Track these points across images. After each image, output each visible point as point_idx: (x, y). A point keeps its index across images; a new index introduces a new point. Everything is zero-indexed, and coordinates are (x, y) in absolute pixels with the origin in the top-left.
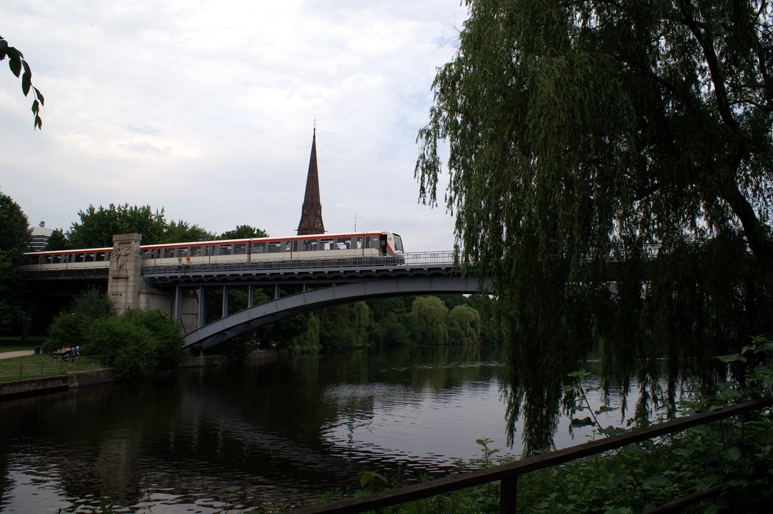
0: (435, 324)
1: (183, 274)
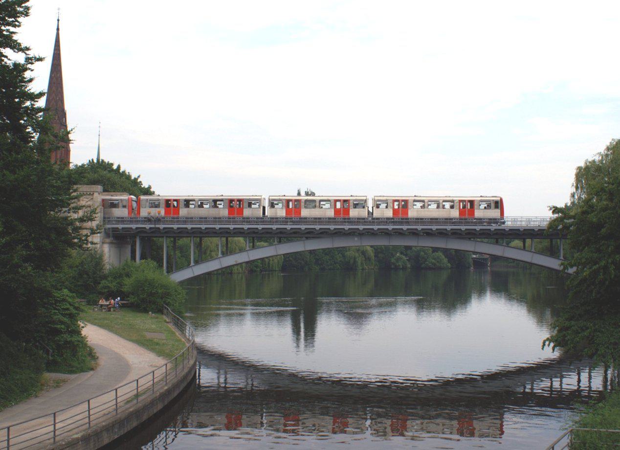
0: (208, 252)
1: (153, 226)
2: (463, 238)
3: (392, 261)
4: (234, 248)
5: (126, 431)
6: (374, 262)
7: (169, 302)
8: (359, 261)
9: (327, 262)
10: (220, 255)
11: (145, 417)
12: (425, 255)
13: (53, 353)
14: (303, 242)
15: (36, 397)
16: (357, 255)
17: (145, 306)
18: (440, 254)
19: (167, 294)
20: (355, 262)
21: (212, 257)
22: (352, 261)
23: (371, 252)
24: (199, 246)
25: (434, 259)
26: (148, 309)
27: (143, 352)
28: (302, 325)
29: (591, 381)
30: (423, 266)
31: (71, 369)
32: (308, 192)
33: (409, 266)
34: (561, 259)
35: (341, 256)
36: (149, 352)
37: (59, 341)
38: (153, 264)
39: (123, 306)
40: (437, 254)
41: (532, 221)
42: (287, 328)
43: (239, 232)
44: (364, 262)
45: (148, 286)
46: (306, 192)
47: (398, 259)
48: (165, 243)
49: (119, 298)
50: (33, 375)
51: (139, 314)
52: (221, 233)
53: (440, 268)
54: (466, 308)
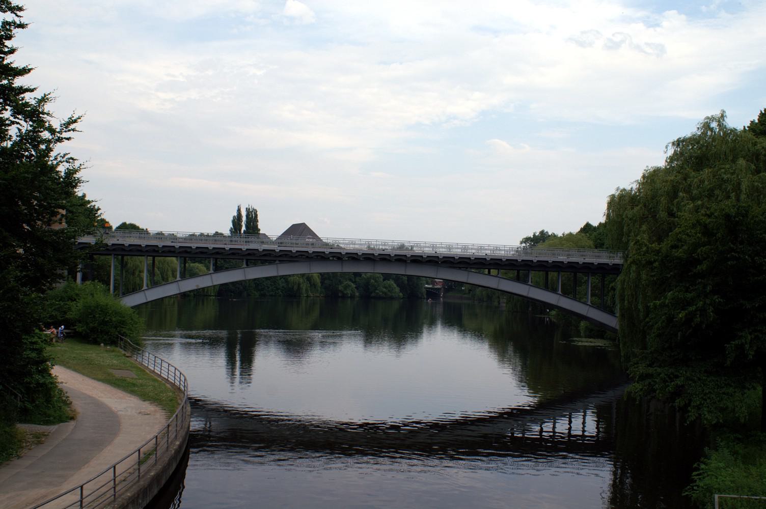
2: (454, 268)
3: (340, 289)
4: (166, 268)
5: (148, 502)
6: (319, 289)
7: (124, 333)
8: (304, 287)
9: (268, 288)
10: (178, 278)
11: (163, 482)
12: (376, 283)
13: (23, 398)
14: (275, 266)
15: (19, 457)
16: (301, 280)
17: (95, 336)
18: (392, 282)
19: (123, 323)
20: (299, 288)
21: (489, 272)
22: (296, 287)
23: (317, 278)
24: (123, 265)
25: (386, 288)
26: (99, 340)
27: (122, 395)
28: (238, 358)
29: (569, 426)
30: (373, 295)
31: (47, 419)
32: (249, 209)
33: (357, 294)
34: (559, 294)
35: (284, 281)
36: (129, 395)
37: (30, 383)
38: (100, 286)
39: (67, 337)
40: (389, 282)
41: (453, 248)
42: (220, 359)
44: (309, 288)
45: (100, 312)
46: (247, 208)
47: (347, 287)
48: (113, 263)
49: (63, 327)
50: (7, 428)
51: (89, 347)
52: (147, 251)
53: (392, 298)
54: (417, 341)
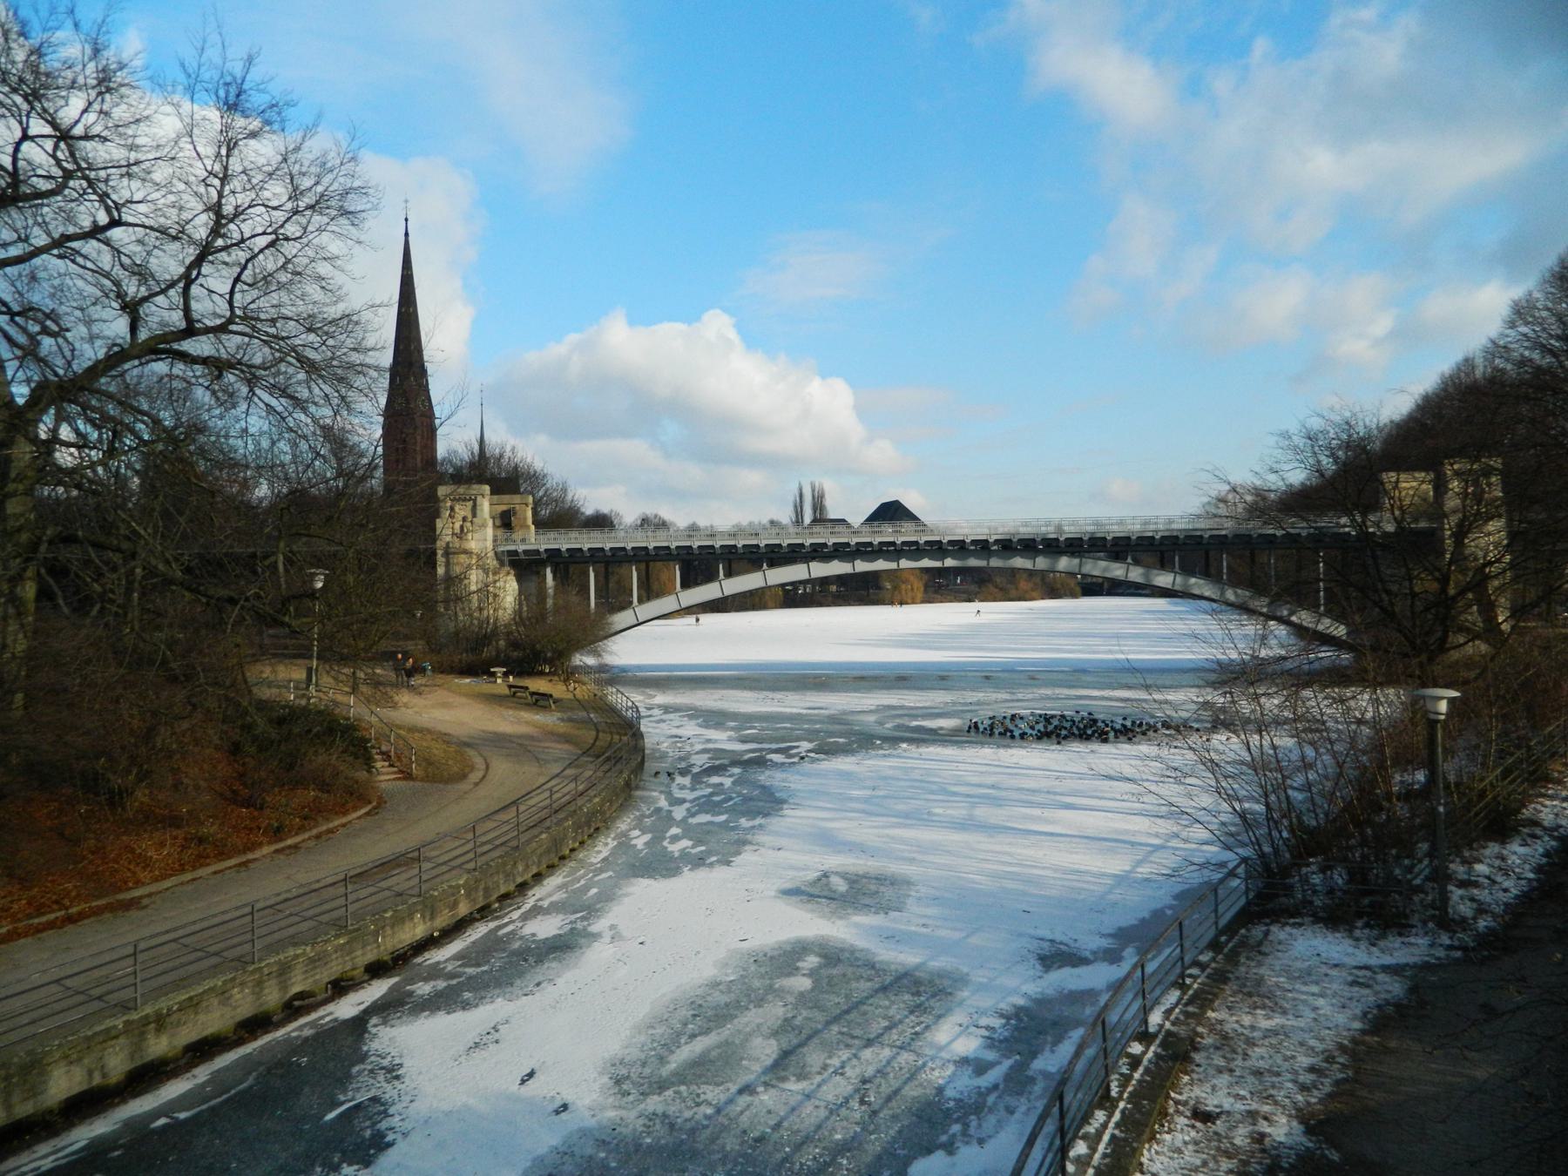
43: (664, 554)
